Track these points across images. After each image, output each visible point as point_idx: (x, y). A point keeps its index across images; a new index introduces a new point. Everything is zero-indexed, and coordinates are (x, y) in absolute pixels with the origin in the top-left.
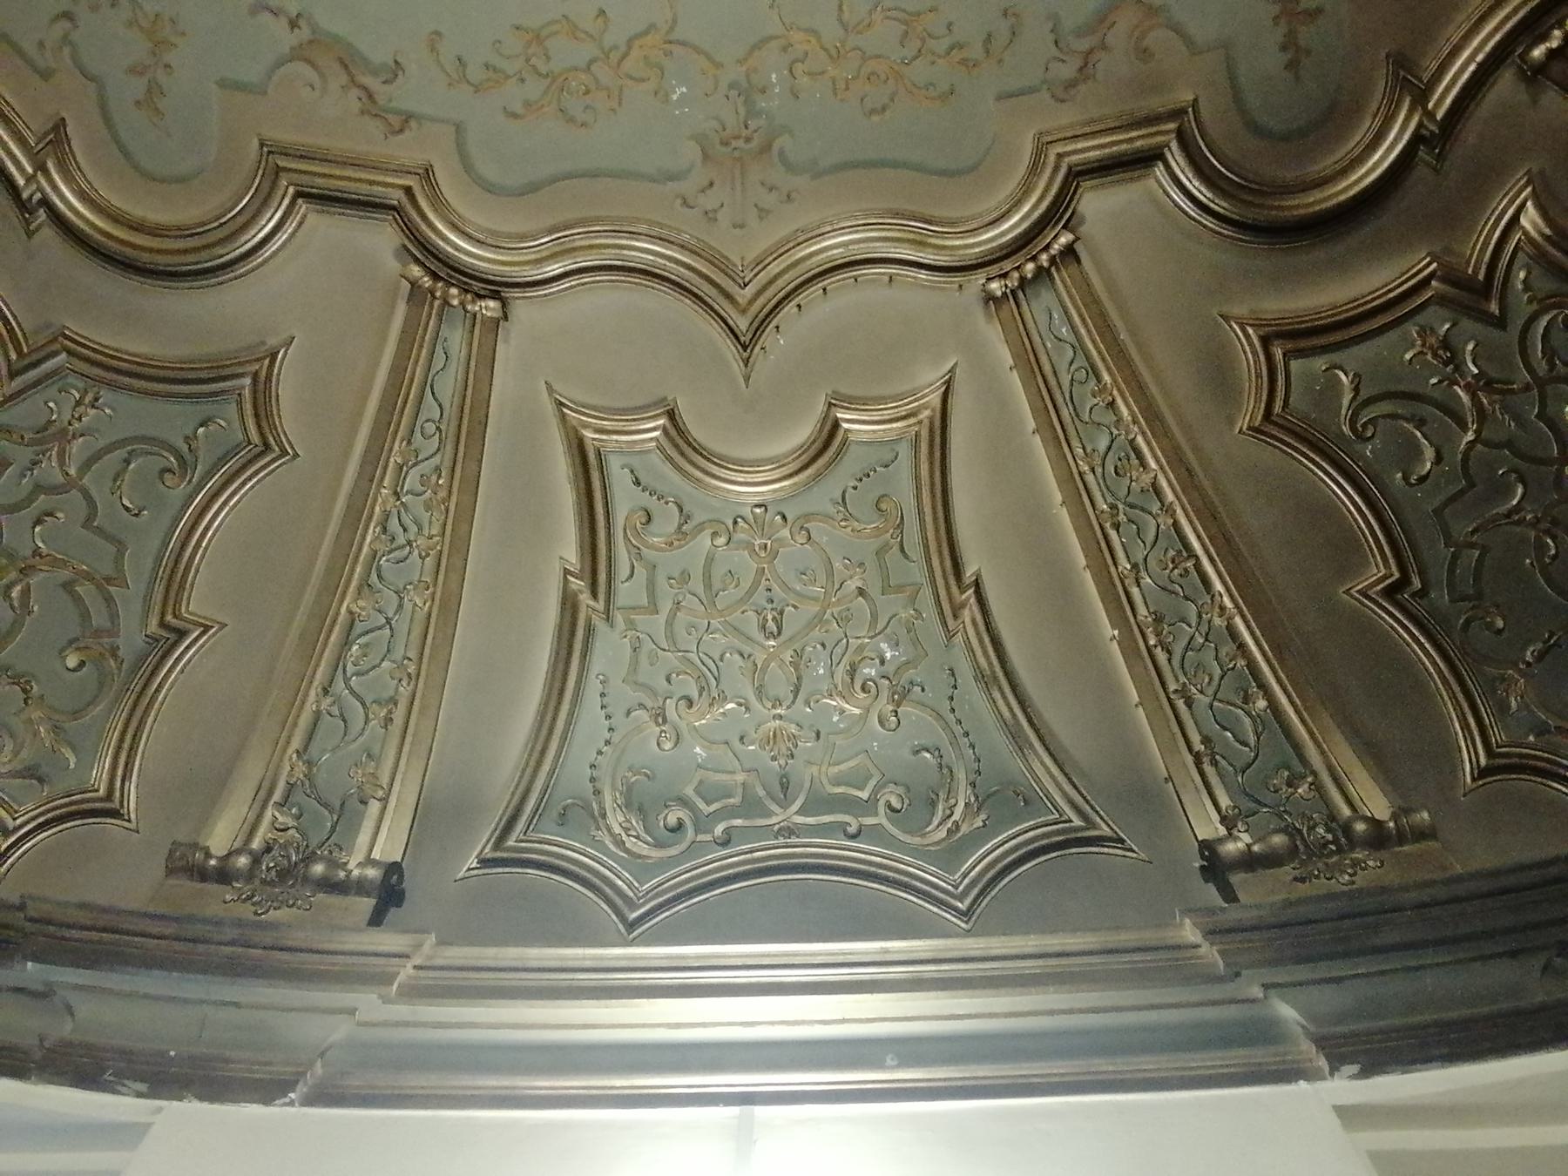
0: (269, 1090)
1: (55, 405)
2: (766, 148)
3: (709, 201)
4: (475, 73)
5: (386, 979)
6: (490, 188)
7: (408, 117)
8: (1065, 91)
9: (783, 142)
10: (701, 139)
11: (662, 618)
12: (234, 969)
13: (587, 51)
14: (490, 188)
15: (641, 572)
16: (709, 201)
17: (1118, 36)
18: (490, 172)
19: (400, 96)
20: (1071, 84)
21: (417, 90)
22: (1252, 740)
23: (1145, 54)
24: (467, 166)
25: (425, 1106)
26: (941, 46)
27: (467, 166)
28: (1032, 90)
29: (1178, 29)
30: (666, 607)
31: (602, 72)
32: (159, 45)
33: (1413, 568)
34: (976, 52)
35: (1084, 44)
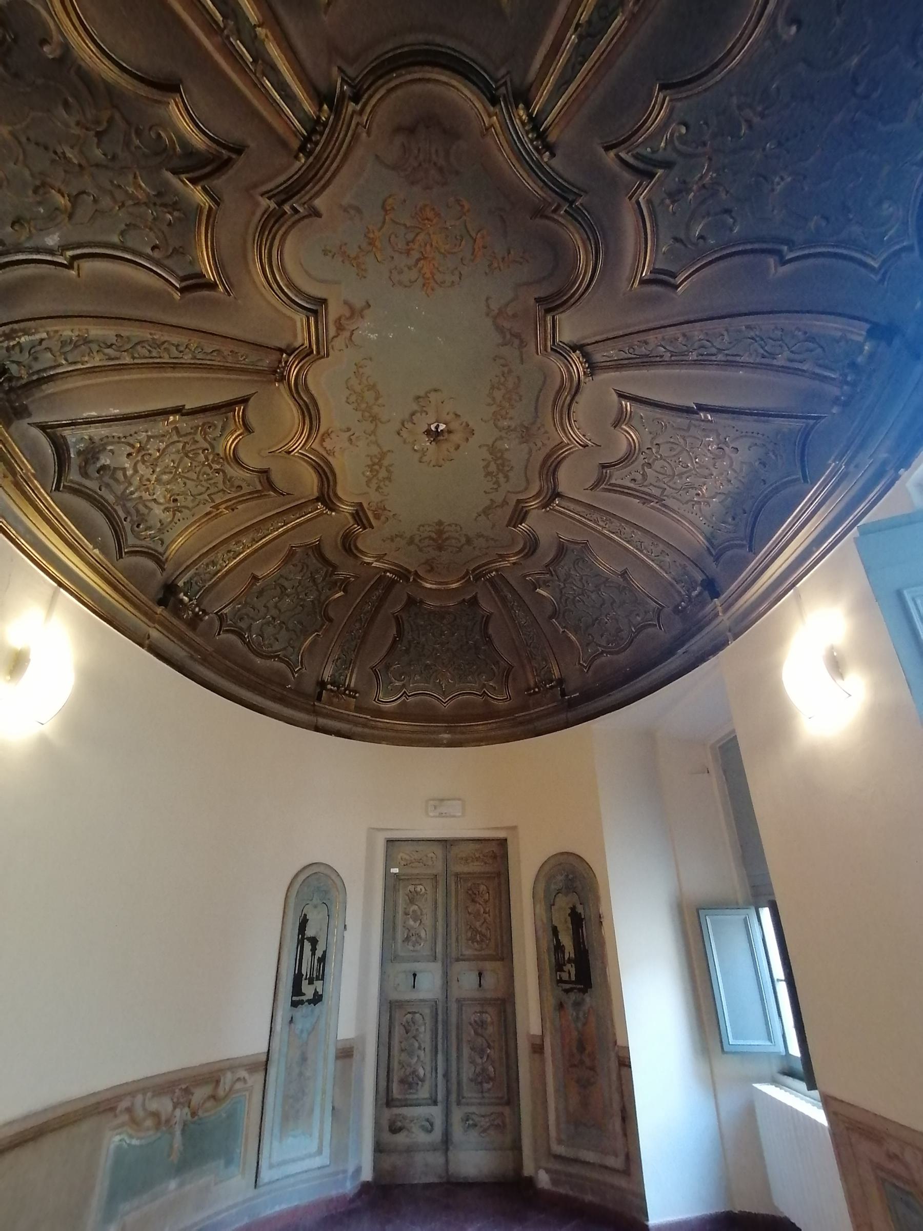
0: (725, 644)
1: (562, 572)
2: (527, 428)
3: (540, 444)
4: (495, 486)
5: (717, 615)
6: (526, 489)
7: (504, 500)
8: (523, 344)
9: (526, 424)
10: (520, 443)
11: (668, 488)
12: (700, 629)
13: (492, 463)
14: (526, 489)
15: (651, 487)
16: (540, 444)
17: (506, 325)
18: (522, 488)
19: (499, 500)
20: (522, 341)
21: (499, 497)
22: (815, 345)
23: (515, 316)
24: (519, 492)
25: (742, 633)
26: (503, 379)
27: (519, 492)
28: (521, 353)
29: (507, 305)
30: (665, 486)
31: (499, 462)
32: (482, 536)
33: (776, 247)
34: (506, 369)
35: (508, 336)
